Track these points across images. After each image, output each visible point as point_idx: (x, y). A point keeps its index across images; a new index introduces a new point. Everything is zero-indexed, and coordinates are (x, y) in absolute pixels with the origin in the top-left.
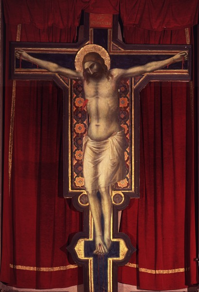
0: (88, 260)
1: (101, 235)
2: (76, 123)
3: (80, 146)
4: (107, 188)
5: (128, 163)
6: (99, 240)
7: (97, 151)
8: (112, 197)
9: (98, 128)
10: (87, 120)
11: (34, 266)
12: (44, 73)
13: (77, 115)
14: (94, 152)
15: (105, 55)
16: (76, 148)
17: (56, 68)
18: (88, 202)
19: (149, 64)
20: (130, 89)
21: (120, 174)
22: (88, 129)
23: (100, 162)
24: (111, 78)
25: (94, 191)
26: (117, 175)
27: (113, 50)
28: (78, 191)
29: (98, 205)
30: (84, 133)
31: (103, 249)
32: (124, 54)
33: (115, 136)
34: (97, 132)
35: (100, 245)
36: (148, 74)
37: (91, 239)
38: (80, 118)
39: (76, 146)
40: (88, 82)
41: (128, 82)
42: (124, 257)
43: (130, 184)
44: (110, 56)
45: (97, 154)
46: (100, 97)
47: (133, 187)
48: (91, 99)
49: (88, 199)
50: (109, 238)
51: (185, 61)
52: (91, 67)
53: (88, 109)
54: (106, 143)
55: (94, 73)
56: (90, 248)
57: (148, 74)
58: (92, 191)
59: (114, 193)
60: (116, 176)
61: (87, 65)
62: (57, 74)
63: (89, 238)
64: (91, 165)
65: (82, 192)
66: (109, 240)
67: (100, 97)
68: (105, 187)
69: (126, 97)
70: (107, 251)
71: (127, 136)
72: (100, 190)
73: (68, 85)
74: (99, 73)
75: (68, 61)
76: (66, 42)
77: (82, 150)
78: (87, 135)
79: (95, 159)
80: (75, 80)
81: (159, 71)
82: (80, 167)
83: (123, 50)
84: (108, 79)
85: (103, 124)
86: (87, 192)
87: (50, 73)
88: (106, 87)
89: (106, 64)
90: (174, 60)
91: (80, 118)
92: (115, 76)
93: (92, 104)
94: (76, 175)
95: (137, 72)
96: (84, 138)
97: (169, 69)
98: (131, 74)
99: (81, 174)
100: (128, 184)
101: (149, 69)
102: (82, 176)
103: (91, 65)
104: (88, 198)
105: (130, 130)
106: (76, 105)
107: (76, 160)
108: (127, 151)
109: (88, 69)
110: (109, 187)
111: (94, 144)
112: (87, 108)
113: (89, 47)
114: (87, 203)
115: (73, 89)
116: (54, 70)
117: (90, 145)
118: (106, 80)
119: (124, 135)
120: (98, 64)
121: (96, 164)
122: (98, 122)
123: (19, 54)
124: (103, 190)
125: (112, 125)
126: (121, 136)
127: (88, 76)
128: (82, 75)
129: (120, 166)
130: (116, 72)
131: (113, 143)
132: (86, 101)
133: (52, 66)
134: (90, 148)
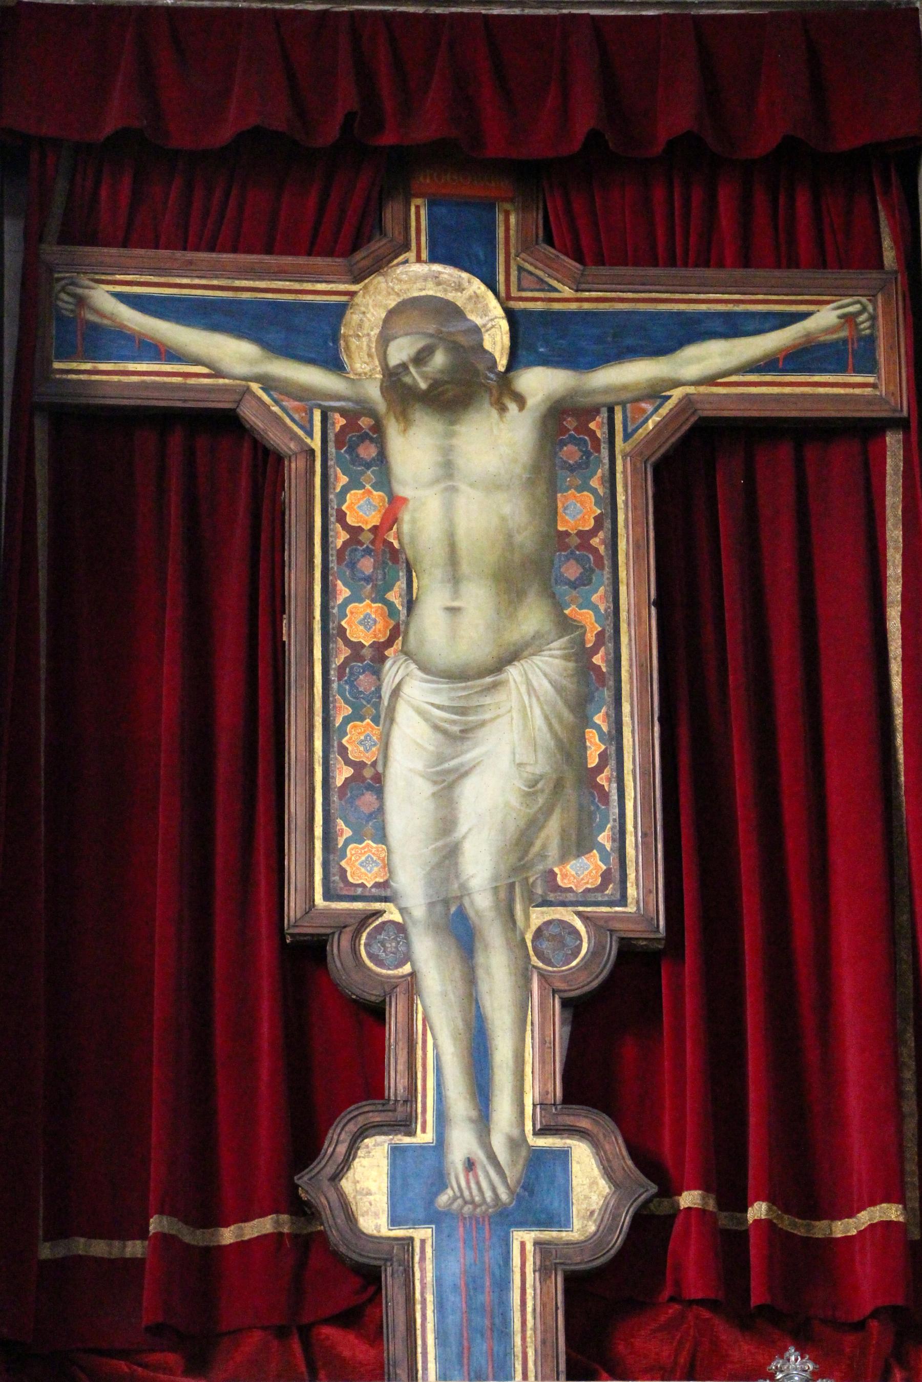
0: (411, 1239)
1: (474, 1114)
2: (347, 602)
3: (377, 709)
4: (503, 895)
5: (602, 779)
6: (462, 1142)
7: (454, 722)
8: (529, 937)
9: (454, 619)
10: (401, 584)
11: (241, 1246)
12: (192, 381)
13: (353, 565)
14: (436, 728)
15: (485, 312)
16: (350, 711)
17: (252, 362)
18: (407, 957)
19: (691, 351)
20: (605, 453)
21: (564, 834)
22: (407, 624)
23: (466, 774)
24: (512, 407)
25: (439, 908)
26: (553, 827)
27: (520, 289)
28: (359, 905)
29: (457, 974)
30: (390, 643)
31: (484, 1184)
32: (574, 306)
33: (536, 659)
34: (453, 634)
35: (470, 1165)
36: (691, 390)
37: (425, 1137)
38: (368, 579)
39: (347, 702)
40: (405, 418)
41: (597, 426)
42: (592, 1228)
43: (616, 876)
44: (511, 315)
45: (457, 732)
46: (460, 484)
47: (631, 891)
48: (420, 493)
49: (408, 944)
50: (515, 1133)
51: (861, 339)
52: (420, 358)
53: (406, 540)
54: (495, 686)
55: (435, 384)
56: (418, 1178)
57: (691, 390)
58: (431, 905)
59: (538, 917)
60: (548, 837)
61: (401, 351)
62: (255, 387)
63: (412, 1133)
64: (425, 789)
65: (379, 913)
66: (516, 1143)
67: (460, 484)
68: (496, 890)
69: (584, 487)
70: (504, 1196)
71: (597, 660)
72: (466, 902)
73: (310, 434)
74: (460, 387)
75: (315, 335)
76: (628, 405)
77: (376, 720)
78: (407, 653)
79: (441, 758)
80: (343, 412)
81: (733, 378)
82: (369, 798)
83: (567, 292)
84: (503, 409)
85: (478, 598)
86: (402, 911)
87: (221, 381)
88: (496, 442)
89: (487, 345)
90: (808, 335)
91: (368, 579)
92: (531, 402)
93: (425, 521)
94: (348, 833)
95: (637, 384)
96: (388, 664)
97: (784, 371)
98: (608, 390)
99: (375, 827)
100: (606, 877)
101: (692, 371)
102: (381, 836)
103: (419, 352)
104: (406, 937)
105: (609, 631)
106: (350, 520)
107: (348, 762)
108: (598, 728)
109: (404, 366)
110: (512, 886)
111: (437, 692)
112: (399, 537)
113: (417, 276)
114: (401, 964)
115: (332, 449)
116: (241, 369)
117: (416, 700)
118: (494, 413)
119: (581, 656)
120: (454, 348)
121: (447, 784)
122: (456, 593)
123: (74, 295)
124: (482, 902)
125: (521, 614)
126: (566, 658)
127: (401, 393)
128: (373, 391)
129: (572, 786)
130: (540, 383)
131: (535, 685)
132: (395, 503)
133: (235, 354)
134: (421, 713)
